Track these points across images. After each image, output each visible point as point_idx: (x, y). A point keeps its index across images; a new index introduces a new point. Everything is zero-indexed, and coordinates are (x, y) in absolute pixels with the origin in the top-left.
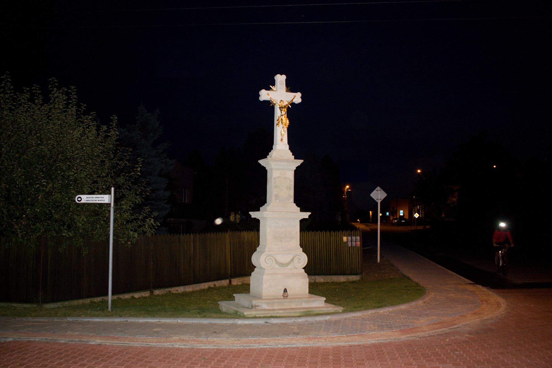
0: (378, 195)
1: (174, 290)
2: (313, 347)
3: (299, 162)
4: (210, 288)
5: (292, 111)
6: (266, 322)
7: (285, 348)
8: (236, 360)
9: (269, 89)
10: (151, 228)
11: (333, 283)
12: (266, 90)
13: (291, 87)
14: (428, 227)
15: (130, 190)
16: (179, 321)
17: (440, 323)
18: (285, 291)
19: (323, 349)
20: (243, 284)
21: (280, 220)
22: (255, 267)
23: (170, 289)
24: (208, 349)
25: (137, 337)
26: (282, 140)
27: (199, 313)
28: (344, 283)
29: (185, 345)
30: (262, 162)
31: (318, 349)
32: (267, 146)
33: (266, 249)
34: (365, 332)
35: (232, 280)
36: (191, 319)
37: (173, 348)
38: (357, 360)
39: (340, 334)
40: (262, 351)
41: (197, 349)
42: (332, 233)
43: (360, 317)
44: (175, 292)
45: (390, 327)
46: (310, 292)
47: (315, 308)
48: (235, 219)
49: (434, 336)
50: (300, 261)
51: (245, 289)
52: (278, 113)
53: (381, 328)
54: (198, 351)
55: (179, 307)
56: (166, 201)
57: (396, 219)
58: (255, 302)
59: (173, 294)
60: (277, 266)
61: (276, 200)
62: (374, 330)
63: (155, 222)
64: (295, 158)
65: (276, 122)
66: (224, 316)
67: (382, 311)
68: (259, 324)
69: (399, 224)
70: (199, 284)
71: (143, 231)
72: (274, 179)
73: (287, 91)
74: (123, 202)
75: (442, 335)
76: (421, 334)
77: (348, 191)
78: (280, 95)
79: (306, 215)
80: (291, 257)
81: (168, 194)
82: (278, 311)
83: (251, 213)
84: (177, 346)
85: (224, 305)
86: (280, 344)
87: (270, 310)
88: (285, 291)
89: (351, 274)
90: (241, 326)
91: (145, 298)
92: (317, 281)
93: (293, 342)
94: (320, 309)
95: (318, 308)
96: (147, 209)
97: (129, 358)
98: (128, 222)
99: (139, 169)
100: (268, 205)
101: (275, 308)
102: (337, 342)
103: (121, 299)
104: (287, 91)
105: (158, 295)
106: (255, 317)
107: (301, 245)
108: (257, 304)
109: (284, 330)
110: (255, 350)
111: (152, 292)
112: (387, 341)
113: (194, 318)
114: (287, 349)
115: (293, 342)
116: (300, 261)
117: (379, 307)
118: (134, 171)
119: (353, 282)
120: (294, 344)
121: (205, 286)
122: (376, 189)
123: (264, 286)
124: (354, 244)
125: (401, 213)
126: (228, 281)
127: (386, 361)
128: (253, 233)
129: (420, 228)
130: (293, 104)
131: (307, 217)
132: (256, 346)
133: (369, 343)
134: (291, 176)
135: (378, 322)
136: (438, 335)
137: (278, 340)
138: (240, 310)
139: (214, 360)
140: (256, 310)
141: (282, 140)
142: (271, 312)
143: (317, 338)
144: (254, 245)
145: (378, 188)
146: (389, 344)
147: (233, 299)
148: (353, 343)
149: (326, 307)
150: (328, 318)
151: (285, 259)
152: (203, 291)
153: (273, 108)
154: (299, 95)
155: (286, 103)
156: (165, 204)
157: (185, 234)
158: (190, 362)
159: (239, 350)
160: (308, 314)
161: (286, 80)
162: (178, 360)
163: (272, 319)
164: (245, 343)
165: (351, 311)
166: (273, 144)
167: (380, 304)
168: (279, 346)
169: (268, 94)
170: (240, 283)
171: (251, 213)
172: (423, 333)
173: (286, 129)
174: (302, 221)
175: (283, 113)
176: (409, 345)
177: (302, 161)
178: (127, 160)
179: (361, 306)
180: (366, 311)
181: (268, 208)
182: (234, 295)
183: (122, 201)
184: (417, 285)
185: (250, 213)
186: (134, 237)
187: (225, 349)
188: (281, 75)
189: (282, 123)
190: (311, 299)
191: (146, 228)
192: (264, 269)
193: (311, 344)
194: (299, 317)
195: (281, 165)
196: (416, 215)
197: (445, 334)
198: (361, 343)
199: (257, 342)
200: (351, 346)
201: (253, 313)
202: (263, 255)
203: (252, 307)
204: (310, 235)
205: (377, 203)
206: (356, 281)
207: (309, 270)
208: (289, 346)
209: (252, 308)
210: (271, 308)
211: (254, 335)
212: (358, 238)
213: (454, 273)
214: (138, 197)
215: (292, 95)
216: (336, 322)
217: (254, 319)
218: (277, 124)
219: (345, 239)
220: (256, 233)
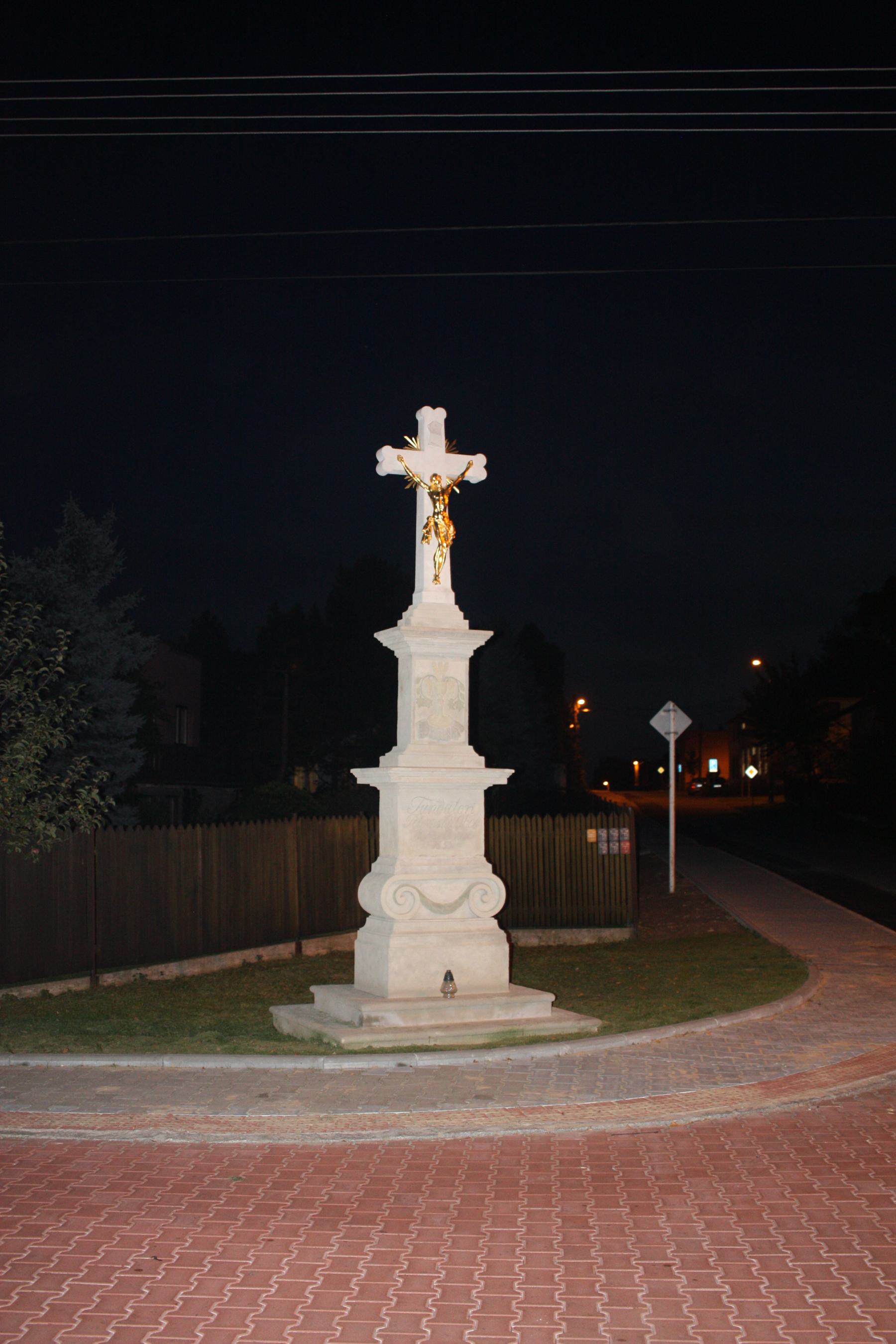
0: (670, 722)
2: (532, 1136)
3: (483, 637)
4: (246, 966)
5: (462, 500)
6: (401, 1065)
7: (455, 1141)
8: (326, 1182)
9: (401, 444)
10: (91, 813)
11: (563, 949)
12: (394, 447)
13: (459, 440)
14: (780, 799)
15: (37, 714)
16: (168, 1062)
17: (860, 1060)
18: (449, 977)
19: (561, 1143)
20: (332, 954)
21: (432, 787)
22: (367, 915)
23: (143, 971)
24: (247, 1147)
25: (52, 1111)
26: (436, 578)
27: (220, 1040)
28: (589, 946)
29: (183, 1136)
30: (384, 637)
31: (547, 1142)
32: (396, 595)
33: (398, 868)
34: (666, 1089)
35: (304, 942)
36: (198, 1057)
37: (150, 1146)
38: (657, 1178)
39: (602, 1097)
40: (394, 1151)
41: (216, 1147)
42: (559, 819)
43: (648, 1045)
44: (155, 978)
45: (732, 1075)
46: (511, 980)
47: (528, 1021)
48: (307, 783)
49: (851, 1099)
50: (485, 898)
51: (341, 969)
52: (425, 507)
53: (707, 1076)
54: (218, 1154)
55: (166, 1021)
56: (132, 741)
57: (699, 781)
58: (368, 1010)
59: (151, 982)
60: (425, 912)
61: (421, 736)
62: (690, 1084)
63: (102, 795)
65: (420, 532)
66: (286, 1046)
67: (703, 1029)
68: (382, 1071)
69: (708, 792)
70: (218, 956)
71: (72, 821)
72: (418, 680)
73: (449, 450)
74: (18, 745)
75: (870, 1095)
76: (816, 1094)
77: (581, 713)
78: (429, 459)
79: (501, 776)
80: (462, 886)
81: (136, 722)
82: (430, 1034)
83: (355, 772)
84: (160, 1139)
85: (285, 1017)
86: (440, 1128)
87: (407, 1030)
88: (449, 977)
90: (332, 1076)
91: (78, 995)
93: (477, 1121)
94: (541, 1026)
95: (536, 1021)
96: (81, 763)
97: (29, 1179)
98: (30, 796)
99: (60, 658)
100: (401, 751)
101: (422, 1024)
102: (596, 1120)
103: (13, 998)
104: (449, 450)
105: (112, 987)
106: (370, 1051)
107: (488, 856)
108: (373, 1015)
109: (451, 1088)
110: (373, 1147)
111: (95, 980)
112: (730, 1116)
113: (206, 1053)
114: (463, 1141)
115: (477, 1121)
116: (485, 898)
117: (696, 1017)
118: (47, 664)
119: (614, 946)
120: (481, 1129)
121: (234, 959)
122: (665, 707)
123: (393, 965)
124: (615, 847)
125: (713, 766)
126: (292, 946)
127: (740, 1180)
128: (356, 821)
129: (761, 801)
130: (463, 484)
131: (504, 782)
132: (377, 1136)
133: (681, 1122)
134: (461, 673)
135: (698, 1058)
136: (863, 1095)
137: (436, 1116)
138: (329, 1032)
139: (264, 1182)
140: (373, 1031)
141: (436, 578)
142: (412, 1035)
143: (539, 1110)
144: (364, 853)
145: (670, 705)
146: (738, 1123)
147: (311, 1000)
148: (640, 1125)
149: (559, 1020)
150: (564, 1049)
151: (444, 891)
152: (229, 972)
153: (412, 495)
154: (480, 460)
155: (445, 482)
156: (131, 747)
157: (181, 827)
158: (196, 1191)
159: (330, 1149)
160: (511, 1039)
161: (446, 421)
162: (164, 1183)
163: (417, 1057)
164: (347, 1126)
165: (624, 1029)
166: (412, 589)
167: (697, 1010)
168: (441, 1135)
169: (400, 459)
170: (323, 952)
171: (355, 772)
172: (823, 1091)
173: (446, 551)
175: (440, 507)
176: (791, 1125)
177: (491, 633)
178: (29, 636)
179: (647, 1016)
180: (663, 1029)
181: (400, 757)
182: (313, 989)
183: (16, 741)
184: (783, 952)
185: (353, 771)
186: (47, 837)
187: (294, 1146)
189: (437, 534)
190: (515, 999)
191: (80, 812)
192: (392, 920)
193: (528, 1127)
194: (489, 1047)
195: (434, 644)
196: (751, 772)
197: (881, 1091)
198: (662, 1124)
199: (378, 1123)
200: (634, 1133)
201: (364, 1039)
202: (389, 881)
203: (361, 1021)
204: (527, 829)
205: (667, 743)
206: (620, 943)
207: (506, 919)
208: (468, 1134)
209: (361, 1024)
210: (410, 1024)
211: (369, 1103)
212: (626, 832)
213: (867, 920)
214: (56, 731)
216: (588, 1062)
217: (367, 1058)
218: (424, 538)
219: (591, 835)
220: (364, 821)
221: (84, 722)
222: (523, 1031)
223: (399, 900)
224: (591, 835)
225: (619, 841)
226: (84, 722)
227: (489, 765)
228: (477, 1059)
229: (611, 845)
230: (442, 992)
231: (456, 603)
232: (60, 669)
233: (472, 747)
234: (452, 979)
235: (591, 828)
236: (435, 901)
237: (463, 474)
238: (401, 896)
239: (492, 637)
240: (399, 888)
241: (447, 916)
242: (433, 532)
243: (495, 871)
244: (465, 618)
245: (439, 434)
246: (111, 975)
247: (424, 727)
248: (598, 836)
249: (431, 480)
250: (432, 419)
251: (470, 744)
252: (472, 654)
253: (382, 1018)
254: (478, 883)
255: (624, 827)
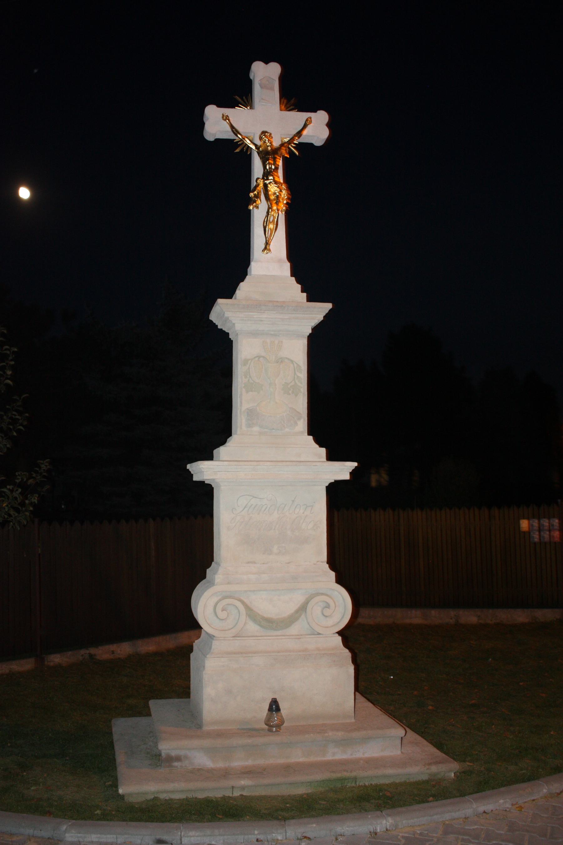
1: (103, 653)
3: (322, 309)
18: (274, 706)
21: (271, 485)
23: (93, 651)
50: (327, 612)
60: (252, 627)
61: (249, 426)
64: (309, 299)
72: (246, 362)
73: (281, 110)
78: (264, 120)
79: (343, 470)
80: (298, 598)
88: (274, 706)
89: (542, 605)
92: (463, 620)
99: (9, 372)
108: (173, 753)
124: (546, 535)
131: (347, 477)
134: (297, 353)
154: (320, 119)
174: (334, 489)
177: (329, 306)
188: (266, 63)
195: (270, 323)
210: (221, 765)
215: (297, 118)
219: (524, 524)
221: (21, 427)
222: (355, 779)
223: (222, 615)
224: (524, 524)
225: (550, 531)
226: (21, 427)
227: (331, 457)
228: (261, 837)
229: (542, 533)
230: (266, 724)
231: (292, 275)
232: (9, 381)
233: (311, 437)
234: (278, 709)
235: (524, 518)
236: (265, 616)
237: (299, 134)
238: (223, 610)
239: (330, 311)
240: (220, 600)
241: (279, 633)
242: (263, 197)
243: (339, 581)
244: (302, 291)
245: (272, 89)
246: (58, 656)
247: (251, 413)
248: (530, 526)
249: (261, 139)
250: (265, 75)
251: (309, 434)
252: (310, 332)
253: (186, 757)
254: (318, 594)
255: (554, 517)
